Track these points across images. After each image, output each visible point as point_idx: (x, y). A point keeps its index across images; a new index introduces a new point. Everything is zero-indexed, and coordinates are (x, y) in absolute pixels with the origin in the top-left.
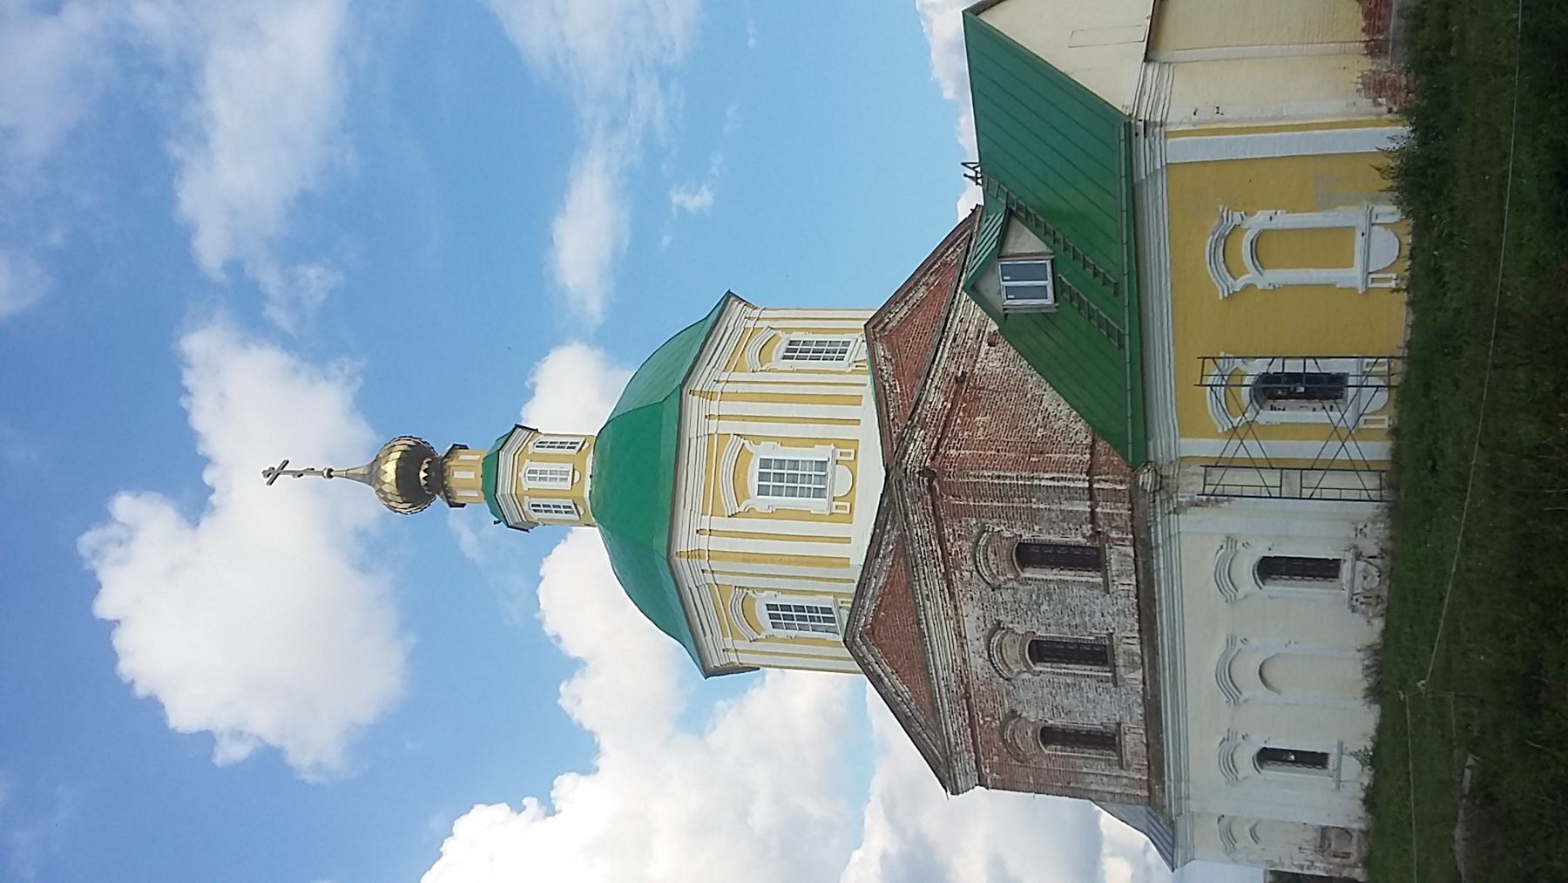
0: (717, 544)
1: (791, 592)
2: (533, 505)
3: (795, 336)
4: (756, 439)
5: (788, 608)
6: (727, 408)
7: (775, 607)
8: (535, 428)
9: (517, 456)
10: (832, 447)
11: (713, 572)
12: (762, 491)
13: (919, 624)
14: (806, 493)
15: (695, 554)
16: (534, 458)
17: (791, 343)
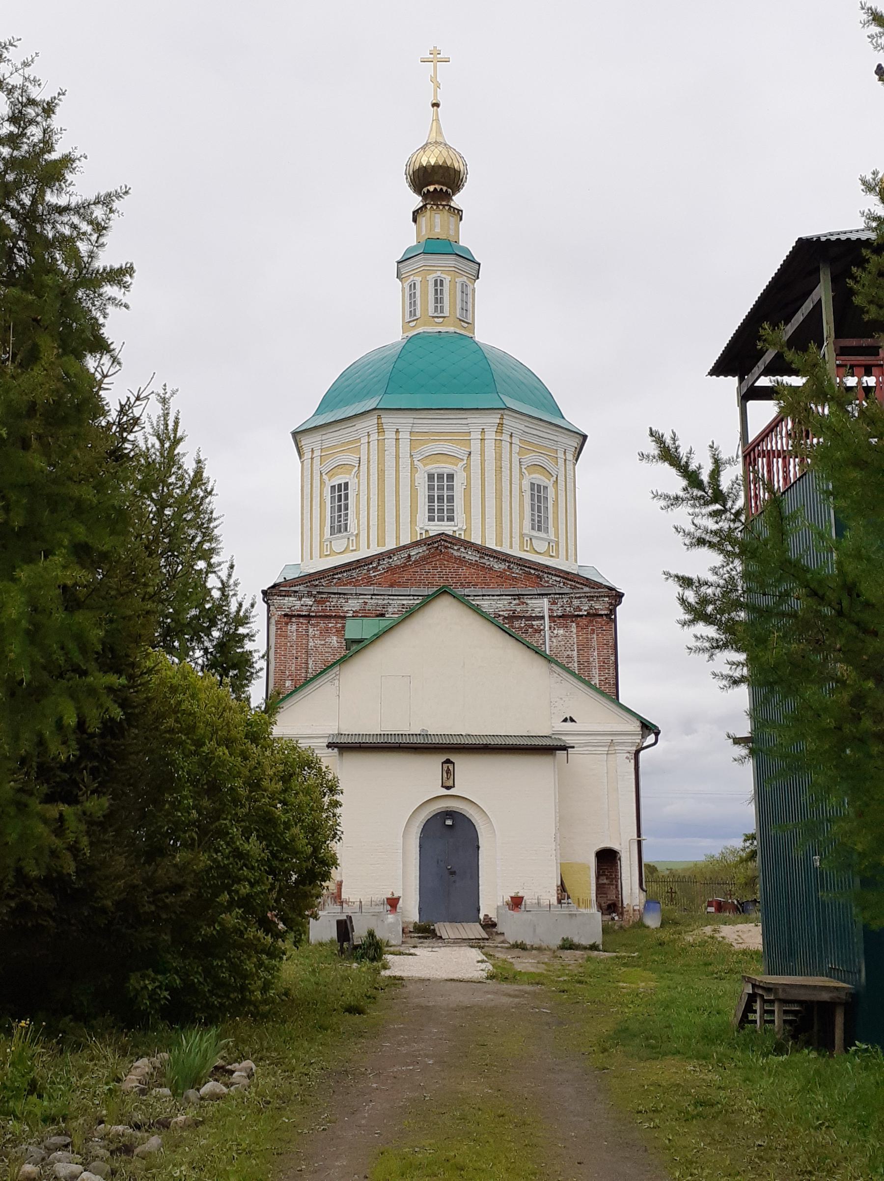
0: (390, 444)
1: (358, 501)
2: (415, 284)
3: (551, 492)
4: (467, 468)
5: (346, 498)
6: (490, 445)
7: (346, 488)
8: (480, 276)
9: (454, 269)
10: (464, 528)
11: (369, 442)
12: (431, 477)
13: (531, 574)
14: (431, 510)
15: (381, 430)
16: (453, 283)
17: (546, 488)
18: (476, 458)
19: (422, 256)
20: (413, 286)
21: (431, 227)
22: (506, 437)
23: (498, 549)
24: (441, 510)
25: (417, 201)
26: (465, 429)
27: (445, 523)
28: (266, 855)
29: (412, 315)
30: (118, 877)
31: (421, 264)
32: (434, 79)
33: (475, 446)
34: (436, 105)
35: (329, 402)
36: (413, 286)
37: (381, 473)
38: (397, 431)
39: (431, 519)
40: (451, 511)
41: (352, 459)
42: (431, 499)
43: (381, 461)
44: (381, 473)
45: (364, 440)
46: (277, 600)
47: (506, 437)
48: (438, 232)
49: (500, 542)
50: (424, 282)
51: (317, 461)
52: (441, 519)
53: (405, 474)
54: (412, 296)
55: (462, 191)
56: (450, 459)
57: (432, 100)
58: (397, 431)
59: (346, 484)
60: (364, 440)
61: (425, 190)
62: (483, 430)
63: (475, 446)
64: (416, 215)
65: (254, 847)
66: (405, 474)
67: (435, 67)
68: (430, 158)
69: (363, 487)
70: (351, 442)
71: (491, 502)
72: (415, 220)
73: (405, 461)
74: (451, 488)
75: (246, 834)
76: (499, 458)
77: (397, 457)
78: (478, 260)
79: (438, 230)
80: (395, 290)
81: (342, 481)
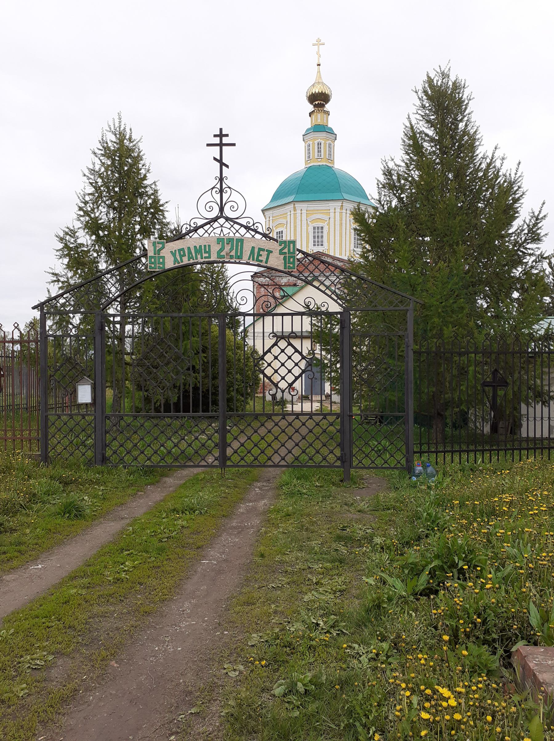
0: (298, 215)
4: (329, 224)
6: (338, 214)
7: (282, 233)
12: (314, 228)
14: (314, 242)
15: (295, 209)
16: (325, 144)
18: (332, 220)
19: (312, 133)
20: (309, 146)
21: (317, 120)
22: (344, 211)
23: (340, 257)
24: (318, 242)
25: (311, 108)
26: (328, 208)
27: (320, 247)
28: (242, 378)
29: (309, 158)
30: (250, 501)
31: (312, 136)
32: (318, 53)
33: (332, 215)
34: (319, 65)
35: (275, 197)
36: (309, 146)
37: (295, 227)
38: (301, 210)
39: (314, 245)
40: (322, 242)
41: (284, 221)
42: (314, 237)
43: (295, 223)
44: (295, 227)
45: (289, 214)
46: (257, 279)
47: (344, 211)
48: (319, 122)
49: (341, 254)
50: (314, 143)
51: (271, 221)
52: (318, 245)
53: (304, 227)
54: (309, 150)
55: (330, 102)
56: (322, 221)
57: (317, 63)
58: (301, 210)
59: (282, 231)
60: (289, 214)
61: (314, 103)
62: (335, 209)
63: (332, 215)
64: (310, 114)
65: (238, 376)
66: (304, 227)
67: (319, 47)
68: (316, 90)
69: (289, 233)
70: (284, 214)
71: (338, 238)
72: (310, 116)
73: (304, 222)
74: (322, 232)
75: (237, 373)
76: (341, 220)
77: (301, 220)
78: (336, 132)
79: (319, 121)
80: (302, 146)
81: (281, 230)
